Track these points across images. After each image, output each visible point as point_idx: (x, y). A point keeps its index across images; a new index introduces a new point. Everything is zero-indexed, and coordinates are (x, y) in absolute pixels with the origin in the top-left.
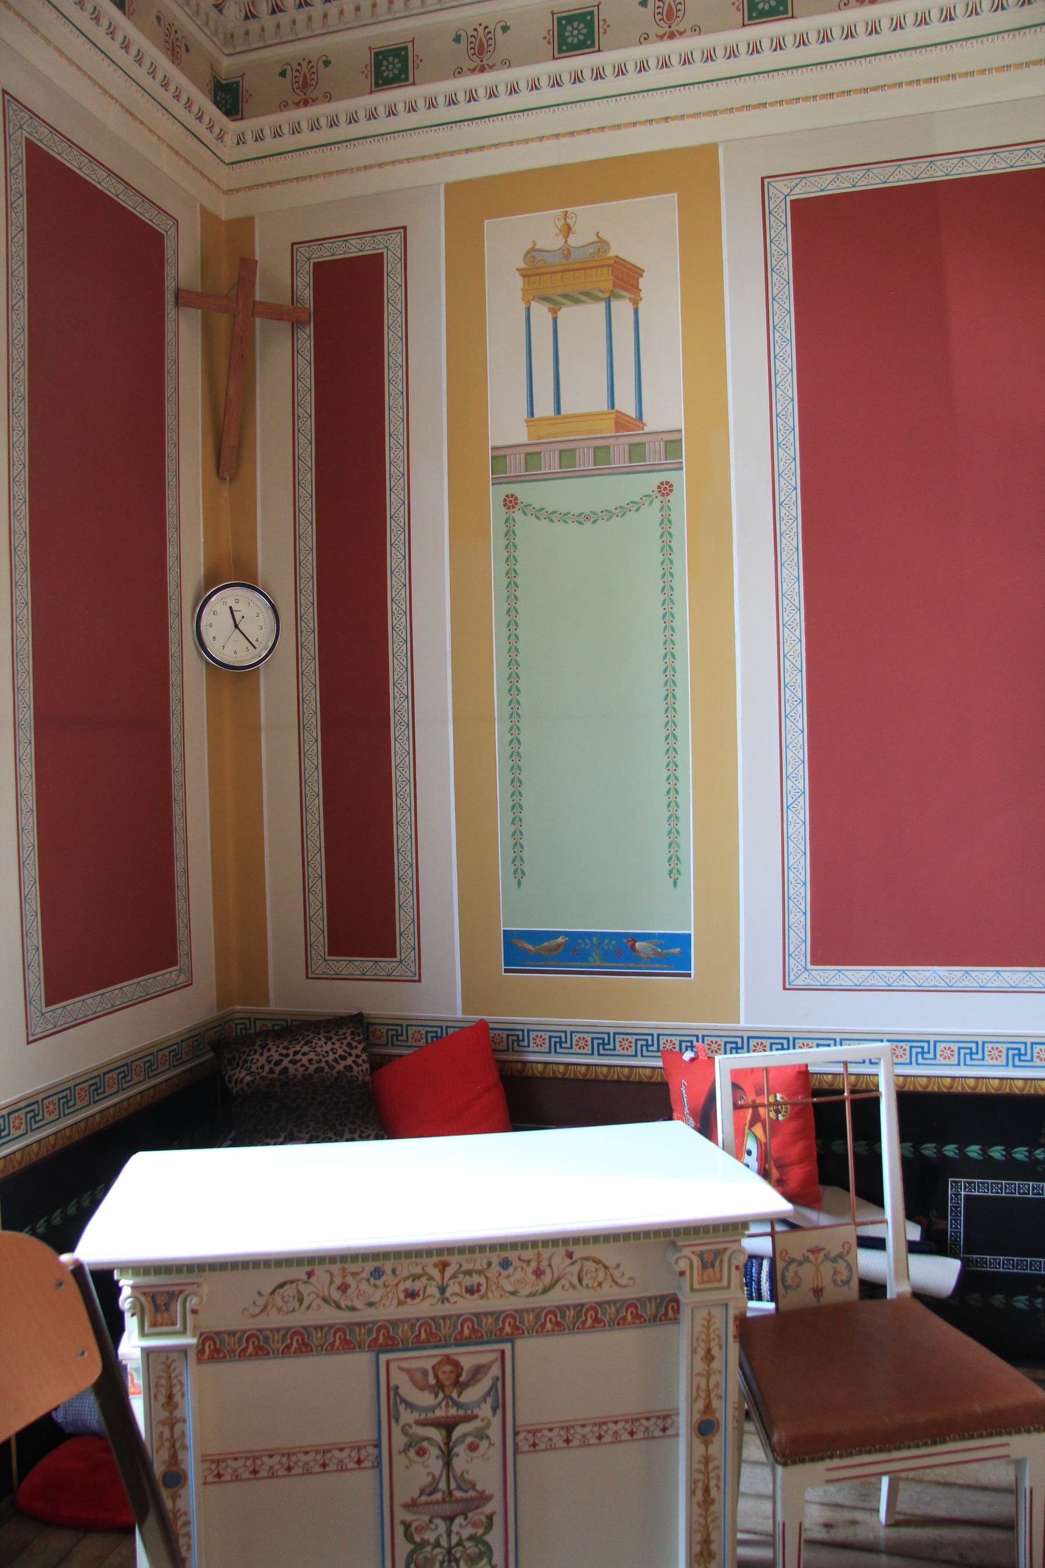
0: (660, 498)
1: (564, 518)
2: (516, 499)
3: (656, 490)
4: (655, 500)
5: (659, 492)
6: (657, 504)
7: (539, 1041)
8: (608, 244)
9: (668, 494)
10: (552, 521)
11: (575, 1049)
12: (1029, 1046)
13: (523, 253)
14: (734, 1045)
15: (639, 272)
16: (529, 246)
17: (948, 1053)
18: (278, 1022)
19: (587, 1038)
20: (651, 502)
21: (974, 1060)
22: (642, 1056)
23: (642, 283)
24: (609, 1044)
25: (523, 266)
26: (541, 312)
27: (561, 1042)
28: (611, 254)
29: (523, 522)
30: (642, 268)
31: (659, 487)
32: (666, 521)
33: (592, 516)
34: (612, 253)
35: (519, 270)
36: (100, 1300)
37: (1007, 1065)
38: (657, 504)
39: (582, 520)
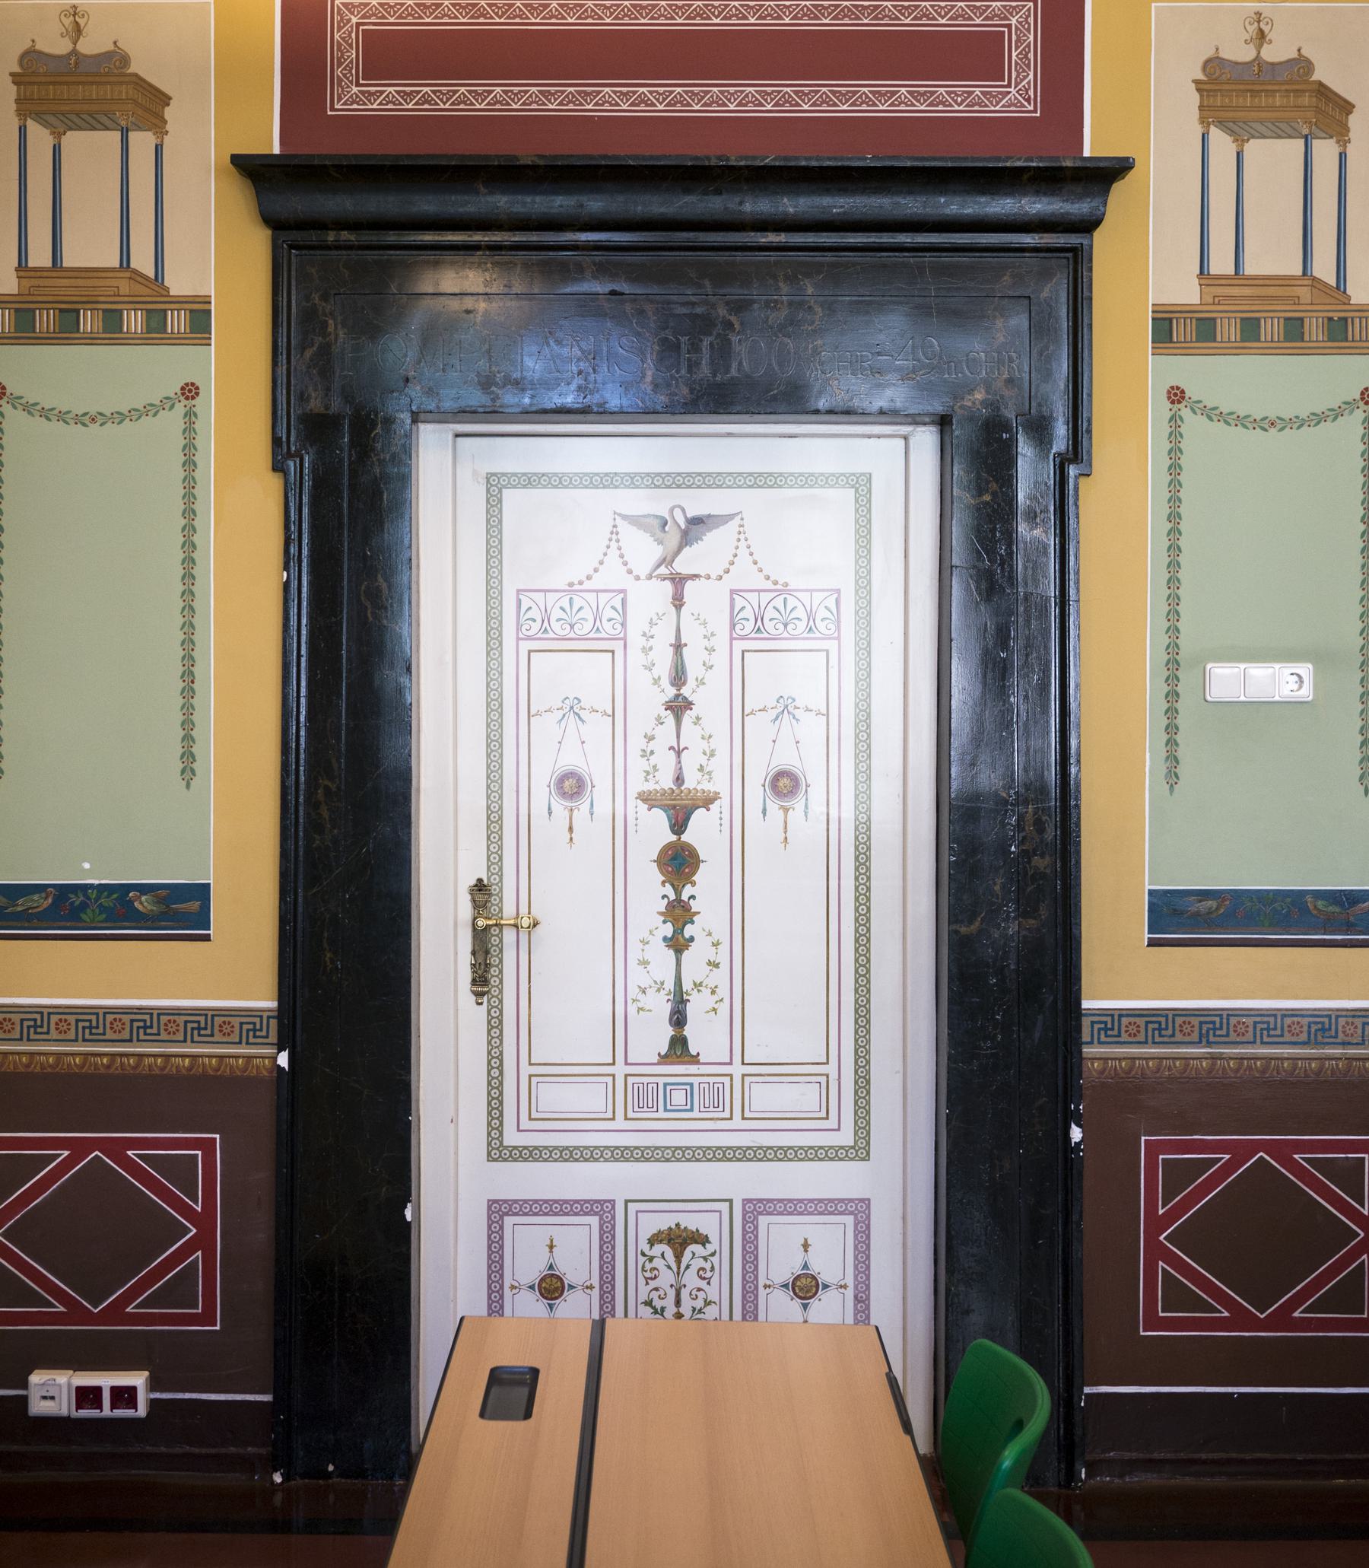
0: (184, 402)
1: (62, 417)
2: (1183, 392)
3: (179, 392)
4: (177, 405)
5: (183, 394)
6: (1186, 413)
7: (63, 1026)
8: (1311, 63)
9: (193, 398)
10: (49, 419)
11: (217, 1037)
12: (155, 1016)
13: (1204, 58)
14: (1163, 1026)
15: (165, 99)
16: (28, 45)
17: (172, 1028)
18: (1154, 1019)
19: (178, 1022)
20: (172, 407)
21: (1163, 1036)
22: (193, 1041)
23: (169, 113)
24: (248, 1031)
25: (1201, 76)
26: (1222, 143)
27: (1160, 1029)
28: (1314, 78)
29: (1193, 424)
30: (1354, 103)
31: (183, 388)
32: (189, 430)
33: (1278, 421)
34: (1315, 77)
35: (1196, 82)
36: (1332, 1337)
37: (185, 1041)
38: (1186, 413)
39: (1266, 426)
